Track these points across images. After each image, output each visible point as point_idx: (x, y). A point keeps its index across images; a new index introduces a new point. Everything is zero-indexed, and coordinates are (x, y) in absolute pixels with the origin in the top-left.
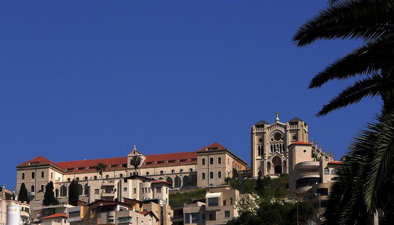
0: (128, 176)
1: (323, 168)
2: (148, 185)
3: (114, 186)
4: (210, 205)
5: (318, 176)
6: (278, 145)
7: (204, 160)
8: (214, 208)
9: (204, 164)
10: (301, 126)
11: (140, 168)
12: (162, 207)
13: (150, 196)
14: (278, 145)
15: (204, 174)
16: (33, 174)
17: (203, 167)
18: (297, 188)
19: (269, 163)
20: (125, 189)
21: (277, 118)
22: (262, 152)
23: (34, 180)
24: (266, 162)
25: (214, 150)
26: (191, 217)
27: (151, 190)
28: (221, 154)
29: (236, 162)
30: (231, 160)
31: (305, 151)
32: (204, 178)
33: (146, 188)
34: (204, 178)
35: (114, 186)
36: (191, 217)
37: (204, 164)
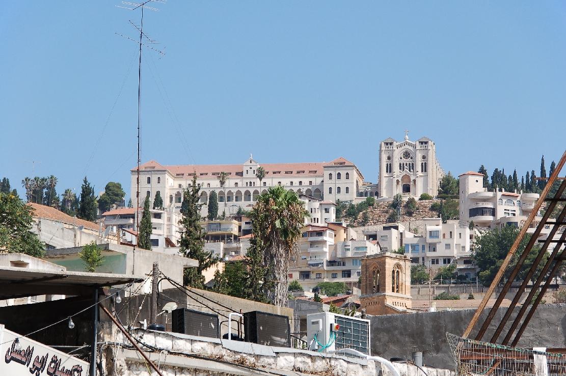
5: (492, 207)
6: (406, 164)
7: (330, 175)
12: (401, 234)
14: (406, 164)
15: (330, 189)
16: (149, 179)
17: (330, 181)
19: (398, 181)
21: (407, 137)
22: (389, 169)
23: (149, 185)
24: (395, 180)
25: (342, 165)
26: (410, 247)
28: (349, 170)
29: (359, 177)
32: (330, 192)
33: (315, 209)
34: (330, 192)
37: (330, 178)
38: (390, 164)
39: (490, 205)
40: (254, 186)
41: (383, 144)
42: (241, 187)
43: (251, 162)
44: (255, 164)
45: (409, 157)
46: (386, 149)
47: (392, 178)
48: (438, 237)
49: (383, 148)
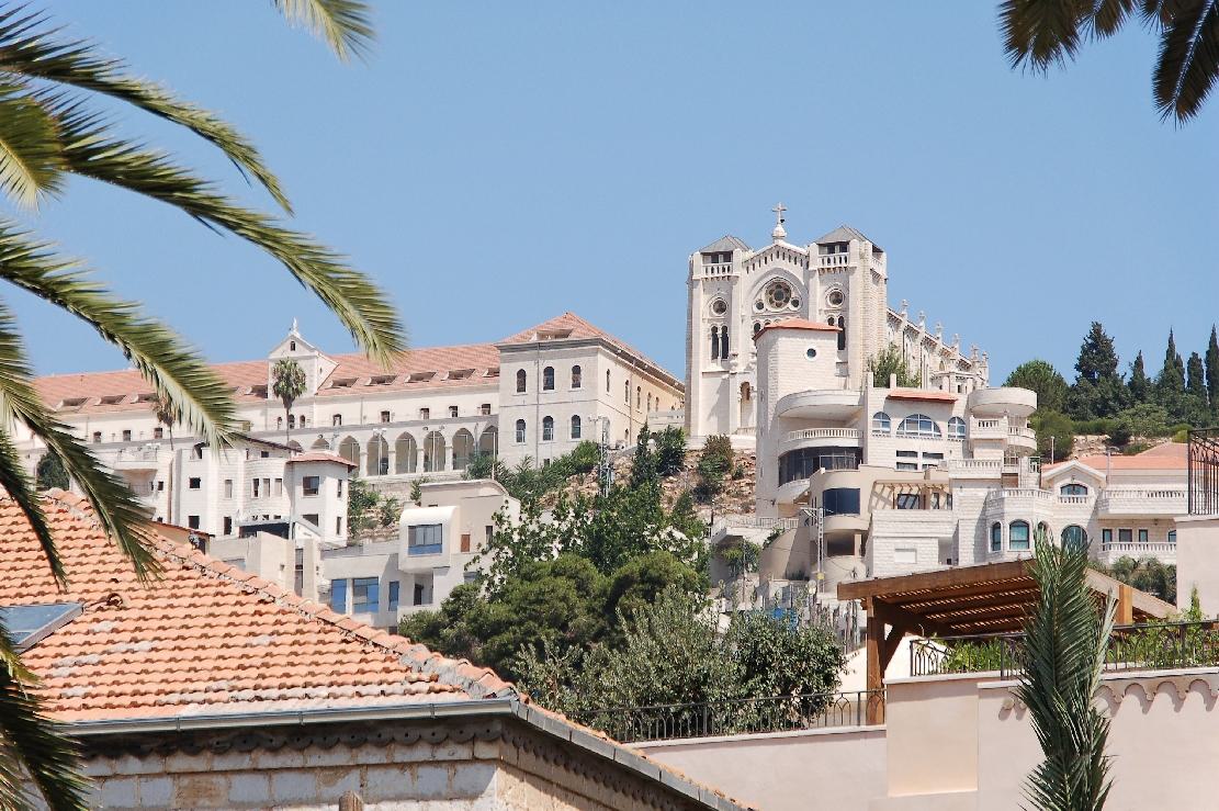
0: (270, 429)
1: (871, 414)
2: (275, 466)
3: (154, 472)
4: (416, 548)
5: (855, 443)
7: (522, 374)
8: (426, 562)
9: (521, 388)
10: (862, 256)
11: (310, 402)
12: (299, 550)
13: (279, 506)
17: (520, 398)
18: (780, 484)
20: (195, 483)
21: (780, 230)
22: (721, 345)
25: (559, 340)
26: (349, 591)
27: (284, 488)
29: (637, 381)
30: (621, 374)
31: (812, 353)
33: (267, 481)
35: (154, 472)
36: (349, 591)
37: (521, 388)
38: (725, 329)
39: (847, 440)
40: (302, 426)
41: (698, 259)
42: (355, 428)
43: (293, 348)
44: (308, 353)
45: (787, 301)
46: (826, 266)
47: (727, 376)
48: (437, 548)
49: (699, 274)
